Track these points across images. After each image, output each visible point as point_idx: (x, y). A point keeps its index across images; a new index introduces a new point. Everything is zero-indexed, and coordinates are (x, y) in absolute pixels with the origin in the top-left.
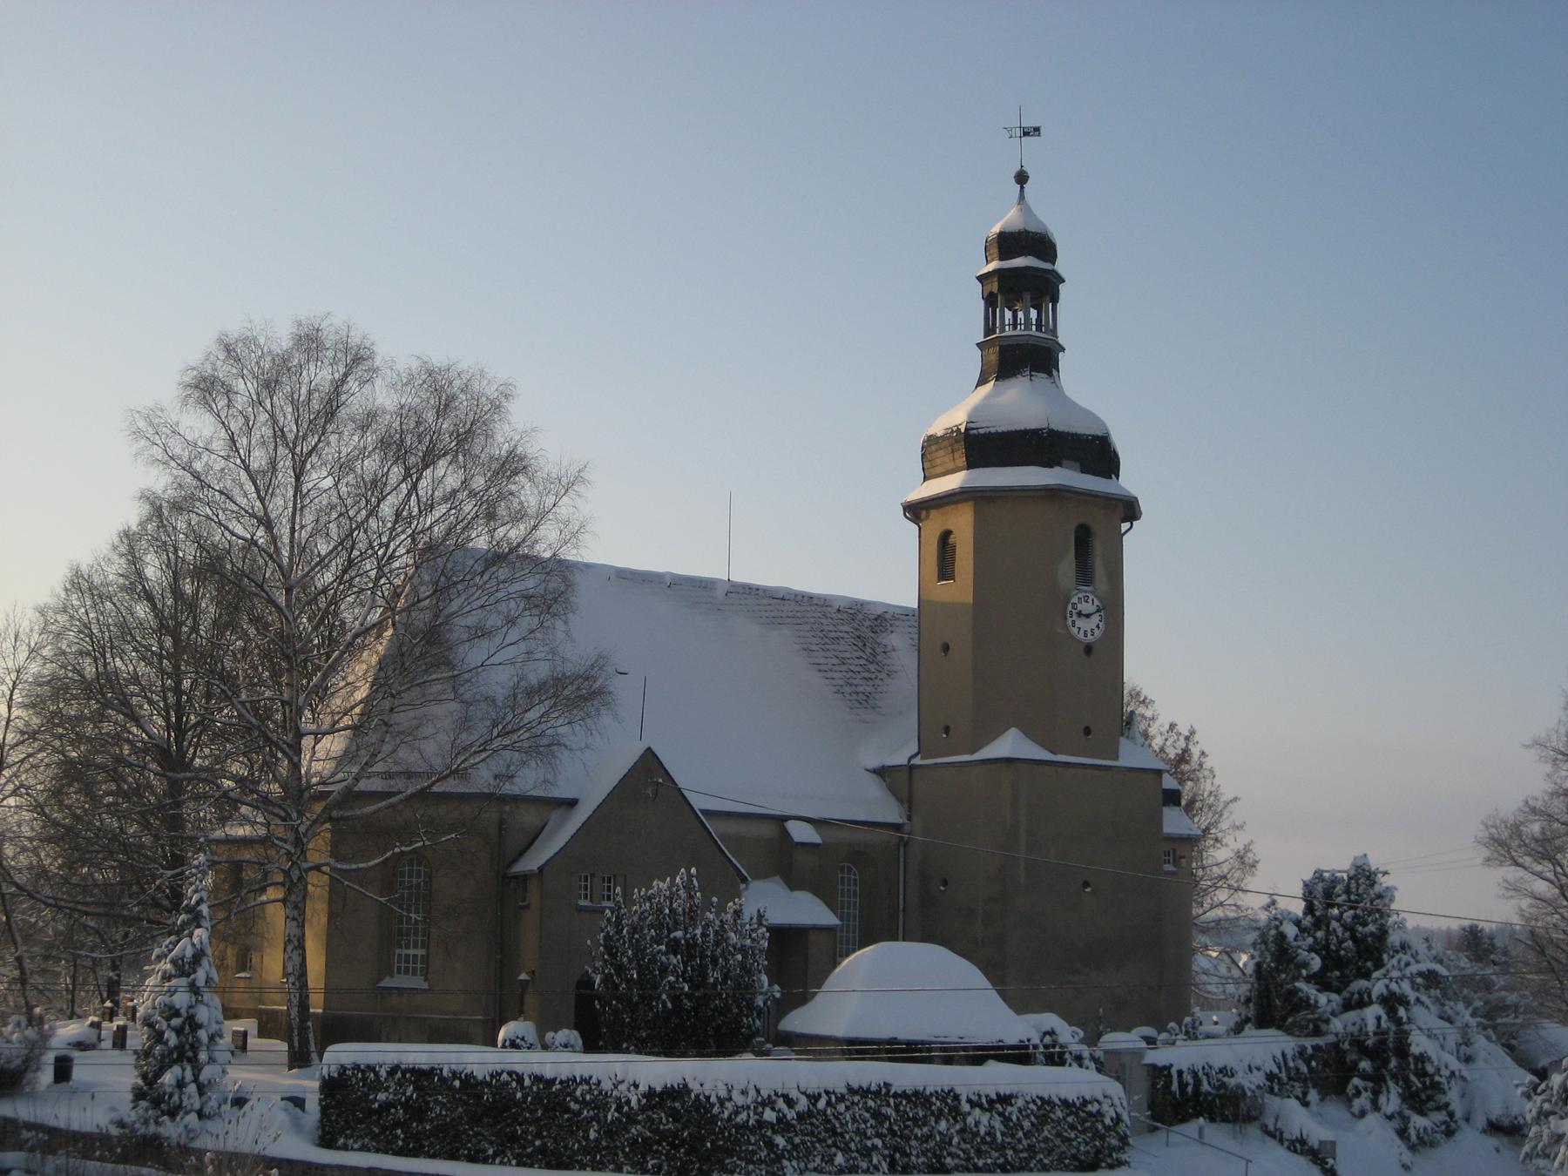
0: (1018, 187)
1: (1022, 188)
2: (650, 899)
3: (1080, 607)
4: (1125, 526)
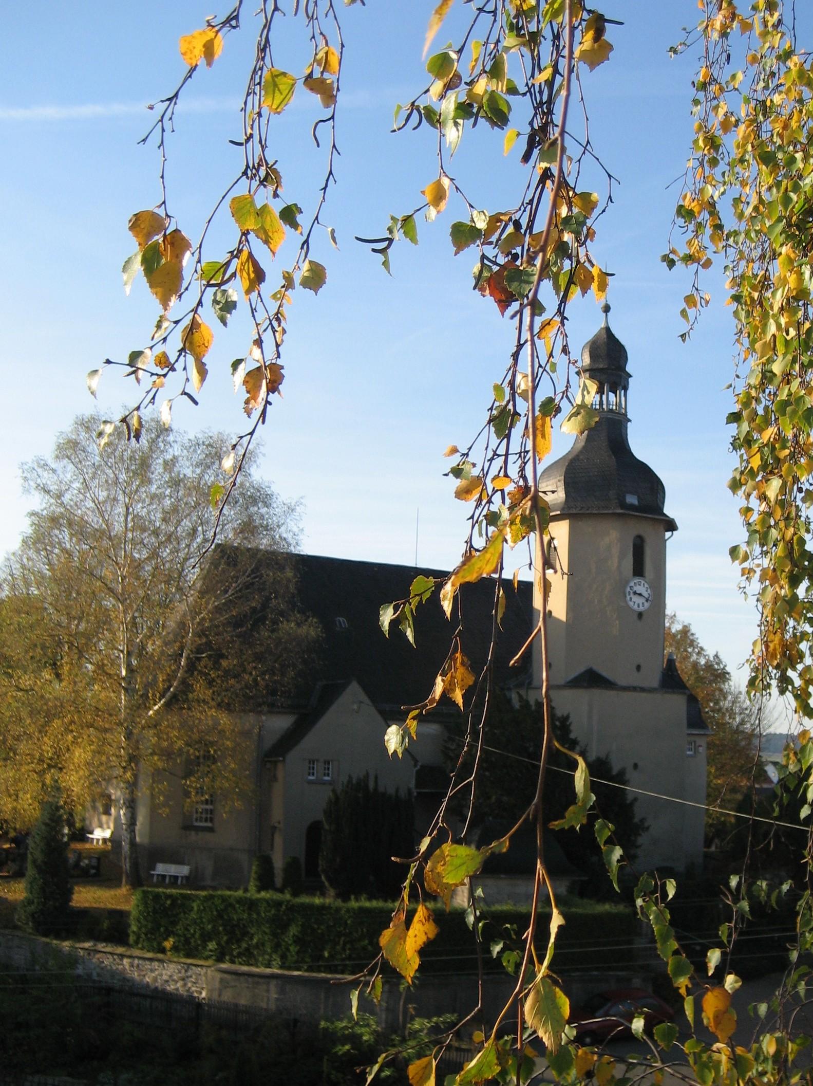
0: (604, 314)
1: (606, 315)
2: (94, 801)
3: (635, 589)
4: (668, 534)
